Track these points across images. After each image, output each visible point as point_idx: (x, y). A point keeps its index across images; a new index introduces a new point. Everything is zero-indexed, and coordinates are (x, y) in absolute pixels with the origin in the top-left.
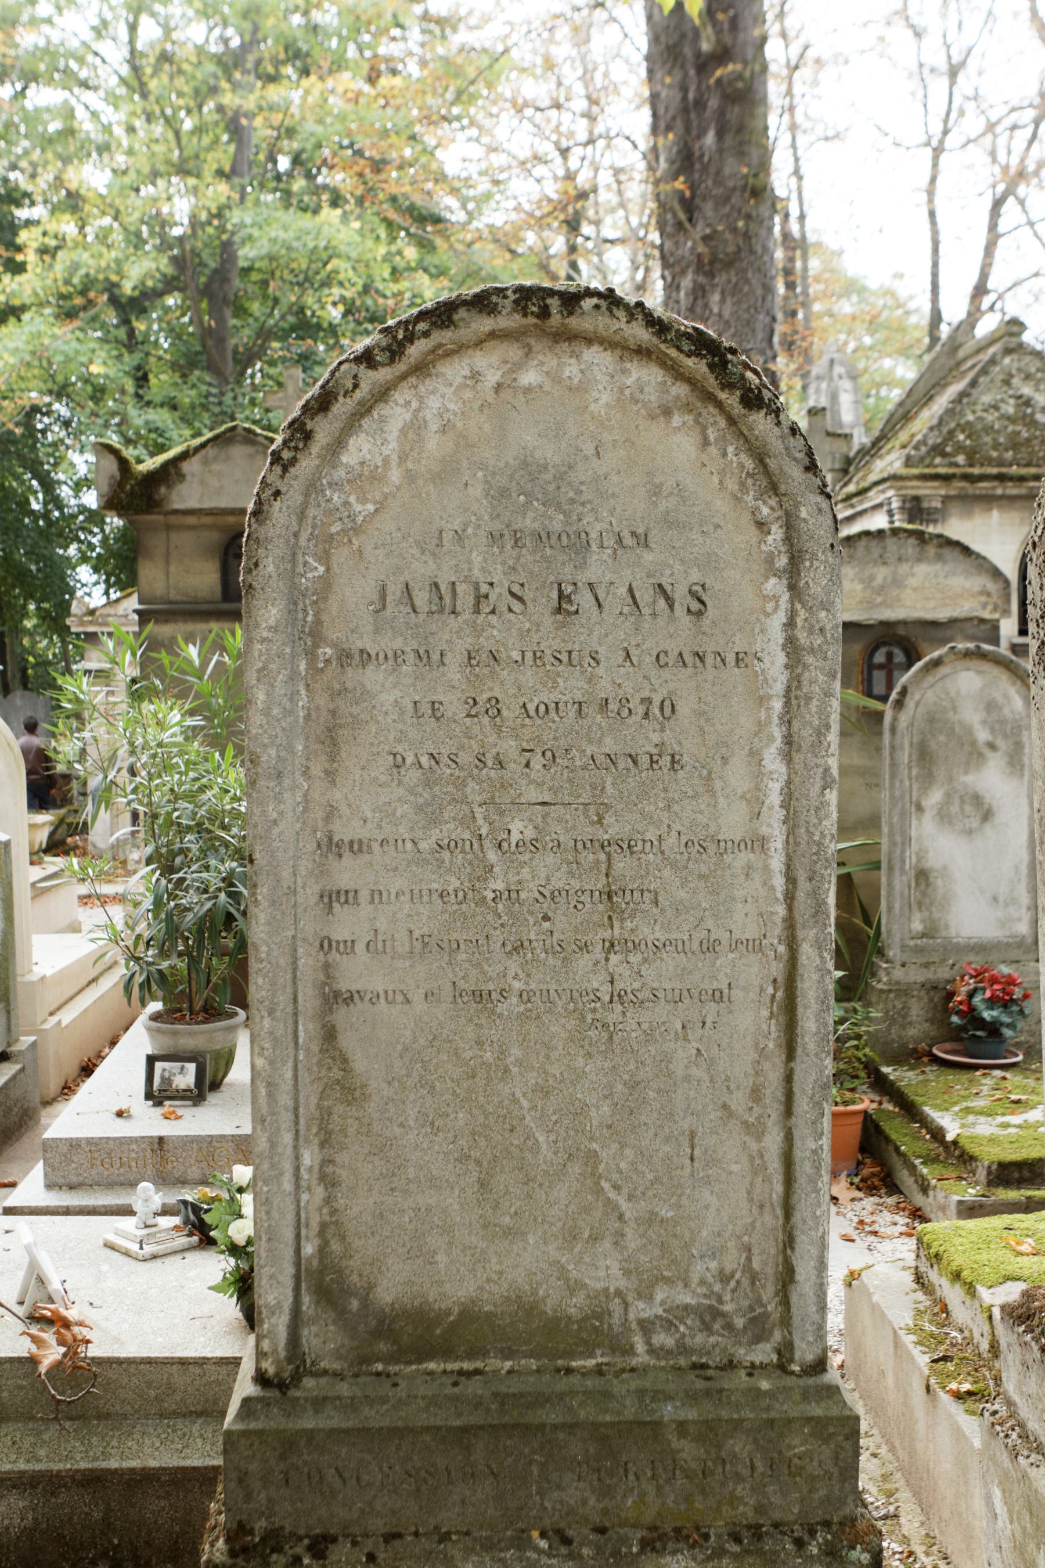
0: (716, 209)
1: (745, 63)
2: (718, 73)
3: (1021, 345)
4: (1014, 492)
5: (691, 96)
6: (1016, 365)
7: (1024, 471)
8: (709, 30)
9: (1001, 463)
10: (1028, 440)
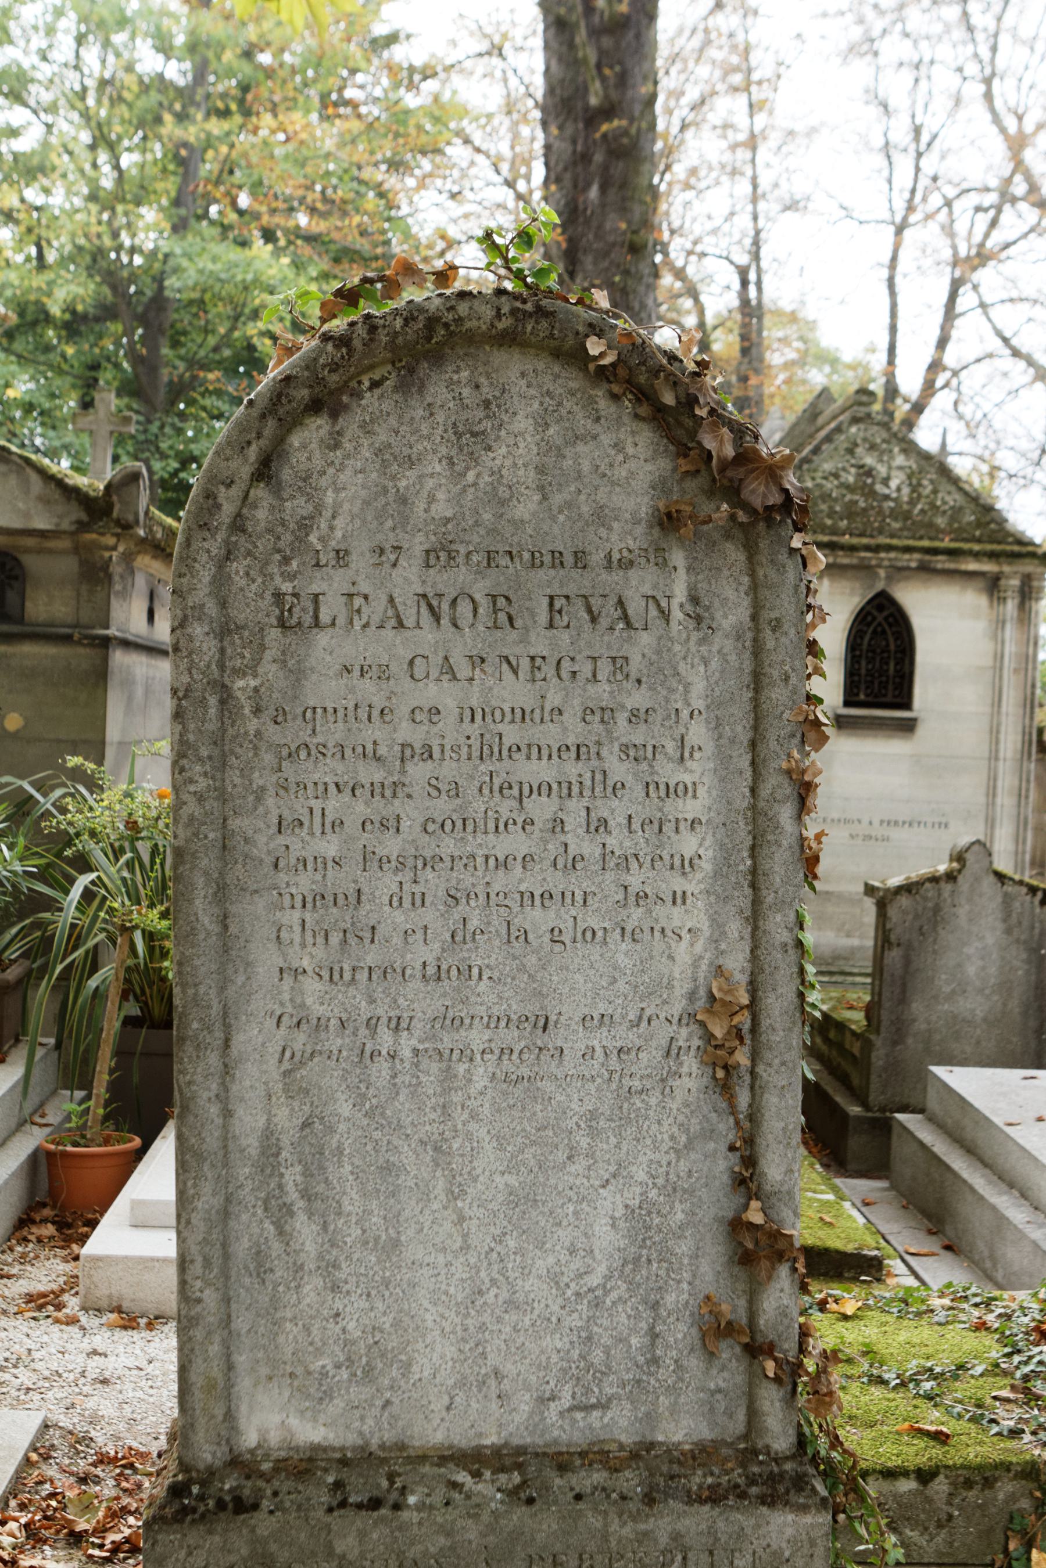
0: (595, 263)
1: (632, 120)
2: (605, 127)
3: (869, 415)
4: (846, 561)
5: (579, 148)
6: (861, 434)
7: (855, 541)
8: (598, 84)
9: (834, 531)
10: (865, 510)
